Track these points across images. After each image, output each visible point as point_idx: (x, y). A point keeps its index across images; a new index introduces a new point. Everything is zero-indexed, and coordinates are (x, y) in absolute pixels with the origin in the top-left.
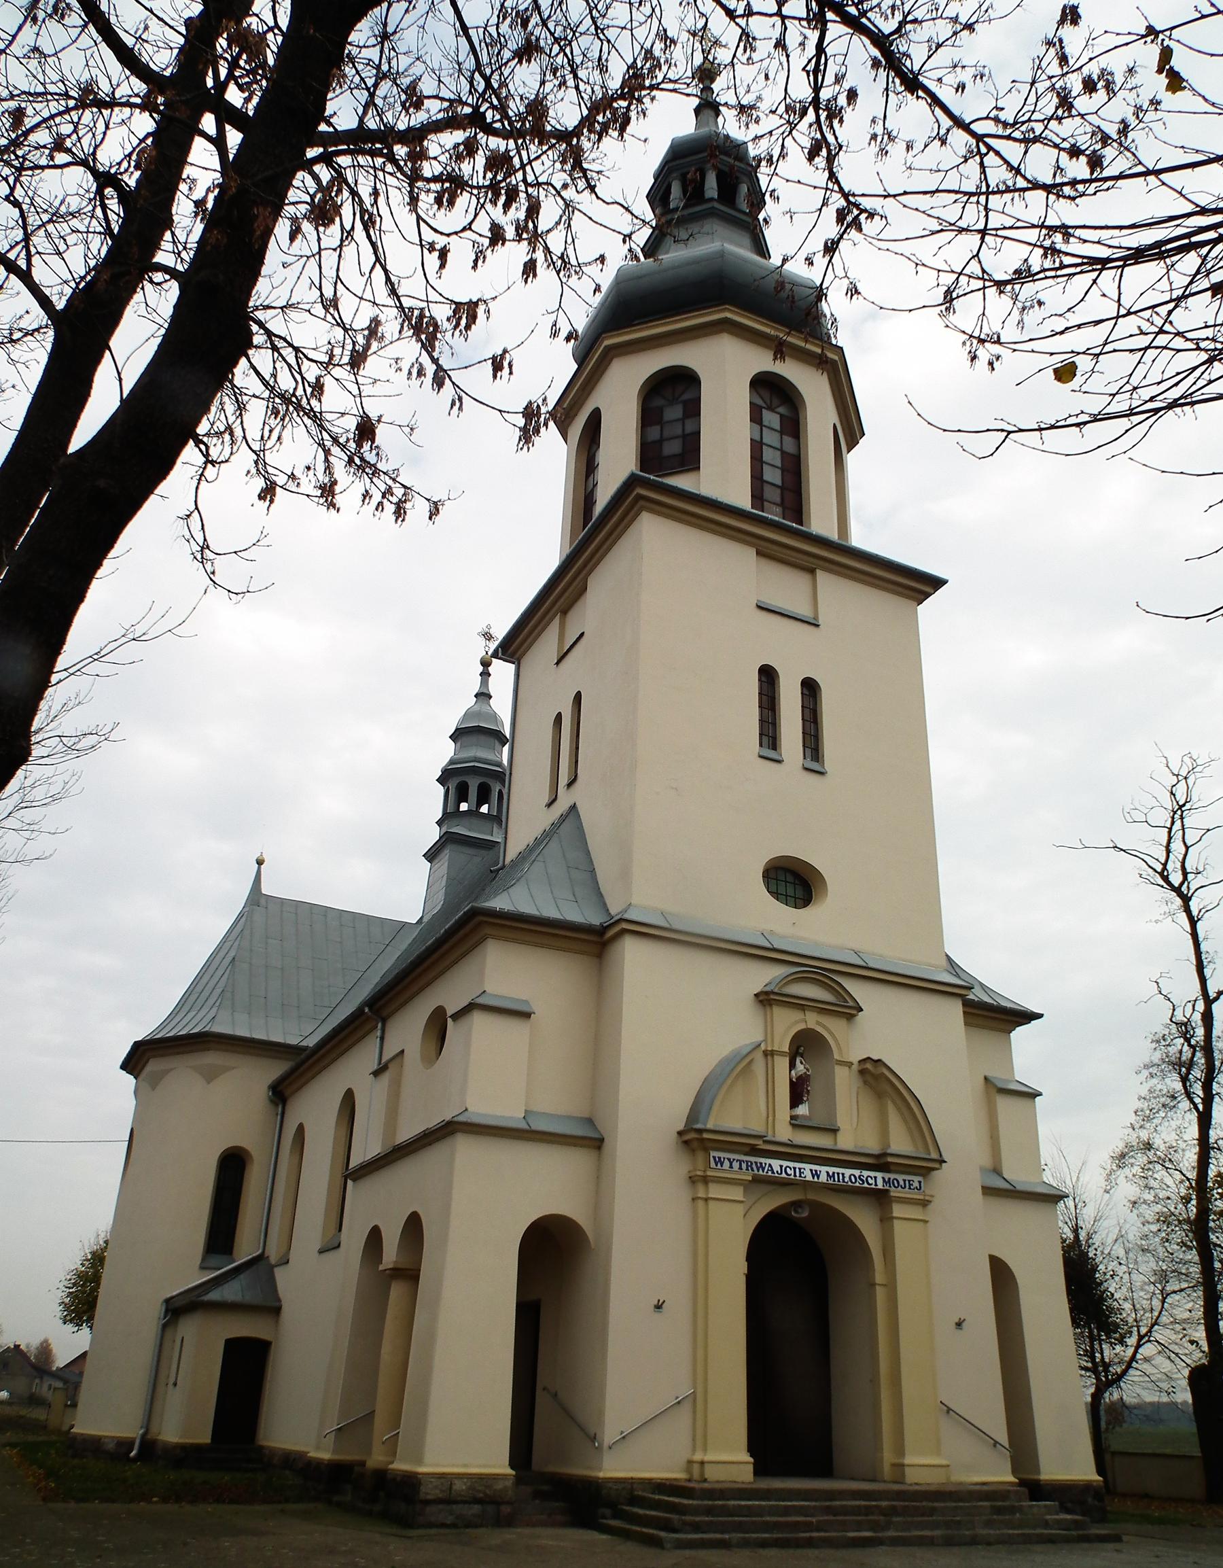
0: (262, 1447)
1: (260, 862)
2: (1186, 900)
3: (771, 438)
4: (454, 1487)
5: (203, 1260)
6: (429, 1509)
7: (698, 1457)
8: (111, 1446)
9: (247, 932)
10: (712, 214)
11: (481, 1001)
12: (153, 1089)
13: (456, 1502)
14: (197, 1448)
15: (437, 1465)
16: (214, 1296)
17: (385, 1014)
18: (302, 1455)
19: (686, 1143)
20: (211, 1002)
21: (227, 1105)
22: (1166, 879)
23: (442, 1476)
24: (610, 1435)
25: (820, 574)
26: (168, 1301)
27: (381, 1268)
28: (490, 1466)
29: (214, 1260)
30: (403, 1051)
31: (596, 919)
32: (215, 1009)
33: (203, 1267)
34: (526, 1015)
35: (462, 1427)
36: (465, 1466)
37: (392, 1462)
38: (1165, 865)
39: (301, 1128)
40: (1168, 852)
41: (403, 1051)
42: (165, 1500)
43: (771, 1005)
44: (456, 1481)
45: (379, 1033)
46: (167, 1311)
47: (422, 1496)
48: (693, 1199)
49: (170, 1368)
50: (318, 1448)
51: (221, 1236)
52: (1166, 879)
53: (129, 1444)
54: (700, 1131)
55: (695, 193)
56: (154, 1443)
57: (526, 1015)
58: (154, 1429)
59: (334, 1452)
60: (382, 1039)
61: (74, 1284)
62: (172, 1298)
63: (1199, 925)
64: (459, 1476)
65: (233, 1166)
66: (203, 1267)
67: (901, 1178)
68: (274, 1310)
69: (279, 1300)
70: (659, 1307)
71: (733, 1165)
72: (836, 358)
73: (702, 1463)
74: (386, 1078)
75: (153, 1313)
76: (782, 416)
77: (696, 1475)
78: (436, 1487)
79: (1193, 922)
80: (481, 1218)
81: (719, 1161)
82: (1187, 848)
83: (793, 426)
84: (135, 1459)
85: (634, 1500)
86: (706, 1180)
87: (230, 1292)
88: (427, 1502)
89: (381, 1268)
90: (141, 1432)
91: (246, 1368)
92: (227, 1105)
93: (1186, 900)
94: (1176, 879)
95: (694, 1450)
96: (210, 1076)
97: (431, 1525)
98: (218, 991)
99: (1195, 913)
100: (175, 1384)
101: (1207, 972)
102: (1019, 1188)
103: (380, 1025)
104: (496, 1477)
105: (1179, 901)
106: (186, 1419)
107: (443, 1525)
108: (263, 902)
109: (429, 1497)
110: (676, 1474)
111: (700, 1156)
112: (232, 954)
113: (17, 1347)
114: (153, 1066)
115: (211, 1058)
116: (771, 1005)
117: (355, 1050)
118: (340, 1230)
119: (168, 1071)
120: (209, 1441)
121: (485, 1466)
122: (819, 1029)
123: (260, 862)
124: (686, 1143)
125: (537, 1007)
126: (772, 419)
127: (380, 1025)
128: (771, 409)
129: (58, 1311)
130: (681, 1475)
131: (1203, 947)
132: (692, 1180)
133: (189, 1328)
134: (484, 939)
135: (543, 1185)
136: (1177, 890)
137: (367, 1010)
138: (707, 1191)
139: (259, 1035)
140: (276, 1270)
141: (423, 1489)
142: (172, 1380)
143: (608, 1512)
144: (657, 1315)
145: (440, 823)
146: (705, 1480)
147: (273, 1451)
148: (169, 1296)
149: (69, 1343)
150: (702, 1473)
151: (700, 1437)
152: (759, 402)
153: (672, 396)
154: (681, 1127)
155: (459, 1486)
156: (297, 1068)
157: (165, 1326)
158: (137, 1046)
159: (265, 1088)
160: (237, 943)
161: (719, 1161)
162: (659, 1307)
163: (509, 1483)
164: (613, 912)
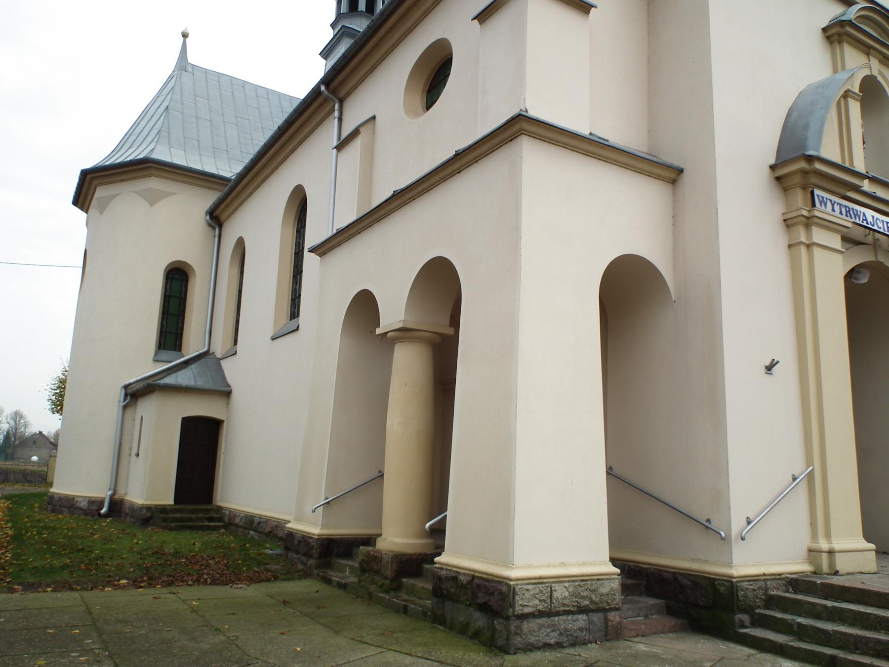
0: (220, 508)
1: (185, 35)
4: (555, 594)
5: (156, 354)
6: (526, 626)
7: (824, 545)
8: (84, 504)
9: (177, 89)
12: (101, 213)
13: (558, 614)
14: (163, 509)
15: (530, 566)
16: (169, 380)
17: (341, 95)
18: (279, 525)
20: (149, 139)
21: (171, 226)
23: (539, 581)
24: (737, 524)
26: (126, 387)
27: (379, 331)
28: (590, 564)
29: (165, 354)
30: (374, 118)
33: (155, 361)
35: (543, 515)
36: (562, 564)
37: (439, 554)
39: (240, 244)
41: (374, 118)
42: (136, 584)
43: (840, 42)
44: (556, 587)
45: (336, 114)
46: (126, 395)
47: (518, 610)
48: (790, 246)
49: (132, 435)
50: (299, 519)
51: (171, 334)
53: (101, 503)
54: (810, 159)
56: (122, 502)
58: (121, 492)
59: (323, 526)
60: (340, 119)
61: (58, 388)
62: (130, 384)
64: (559, 579)
65: (177, 278)
66: (155, 361)
68: (227, 394)
69: (229, 386)
71: (830, 207)
73: (831, 552)
74: (356, 146)
75: (117, 396)
77: (825, 568)
78: (534, 596)
80: (545, 254)
84: (106, 516)
85: (771, 601)
86: (809, 222)
87: (183, 378)
88: (523, 617)
89: (379, 331)
90: (110, 493)
91: (201, 444)
92: (171, 226)
95: (814, 536)
96: (153, 199)
97: (530, 648)
98: (155, 131)
100: (138, 455)
103: (337, 106)
104: (599, 578)
106: (151, 482)
107: (547, 646)
108: (189, 68)
109: (527, 610)
110: (798, 566)
113: (41, 433)
114: (101, 193)
115: (153, 183)
116: (840, 42)
117: (294, 157)
118: (294, 312)
119: (117, 195)
120: (172, 503)
121: (584, 564)
122: (880, 78)
123: (185, 35)
127: (337, 106)
129: (48, 405)
130: (806, 568)
132: (788, 223)
133: (148, 407)
135: (618, 218)
137: (323, 88)
138: (809, 234)
139: (197, 166)
140: (224, 363)
141: (519, 601)
142: (134, 451)
143: (745, 618)
145: (333, 25)
146: (836, 573)
147: (233, 514)
148: (127, 383)
149: (44, 422)
150: (832, 564)
151: (819, 520)
154: (772, 161)
155: (561, 592)
156: (227, 197)
157: (125, 407)
158: (85, 175)
160: (169, 96)
163: (616, 584)
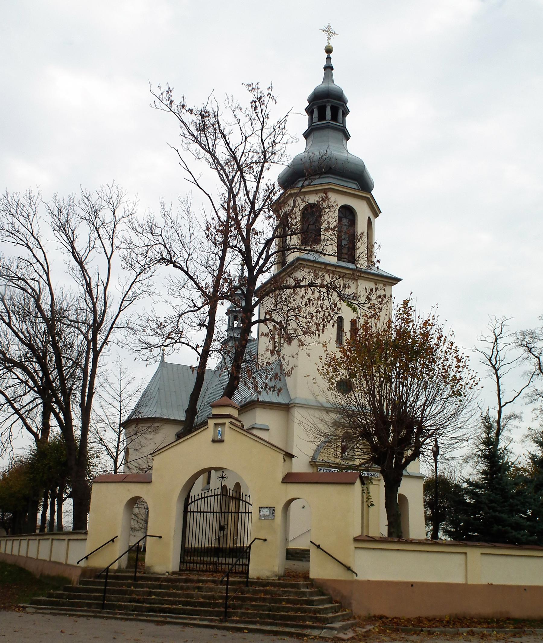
2: (496, 371)
3: (345, 229)
10: (327, 127)
11: (255, 426)
19: (311, 465)
22: (490, 360)
25: (359, 281)
31: (286, 401)
32: (155, 408)
34: (268, 430)
38: (491, 358)
40: (493, 352)
52: (490, 360)
54: (315, 462)
55: (322, 117)
57: (268, 430)
63: (500, 380)
67: (372, 473)
70: (303, 507)
72: (369, 196)
76: (349, 220)
79: (498, 379)
81: (320, 470)
82: (498, 352)
83: (353, 222)
85: (296, 553)
93: (496, 371)
94: (494, 362)
99: (499, 375)
101: (501, 396)
102: (411, 474)
105: (494, 371)
108: (165, 365)
111: (315, 468)
112: (158, 387)
124: (311, 465)
125: (270, 427)
126: (345, 221)
128: (346, 217)
131: (500, 388)
134: (256, 408)
136: (494, 367)
144: (303, 509)
152: (342, 216)
153: (313, 213)
159: (174, 435)
161: (320, 470)
162: (303, 507)
164: (292, 398)
